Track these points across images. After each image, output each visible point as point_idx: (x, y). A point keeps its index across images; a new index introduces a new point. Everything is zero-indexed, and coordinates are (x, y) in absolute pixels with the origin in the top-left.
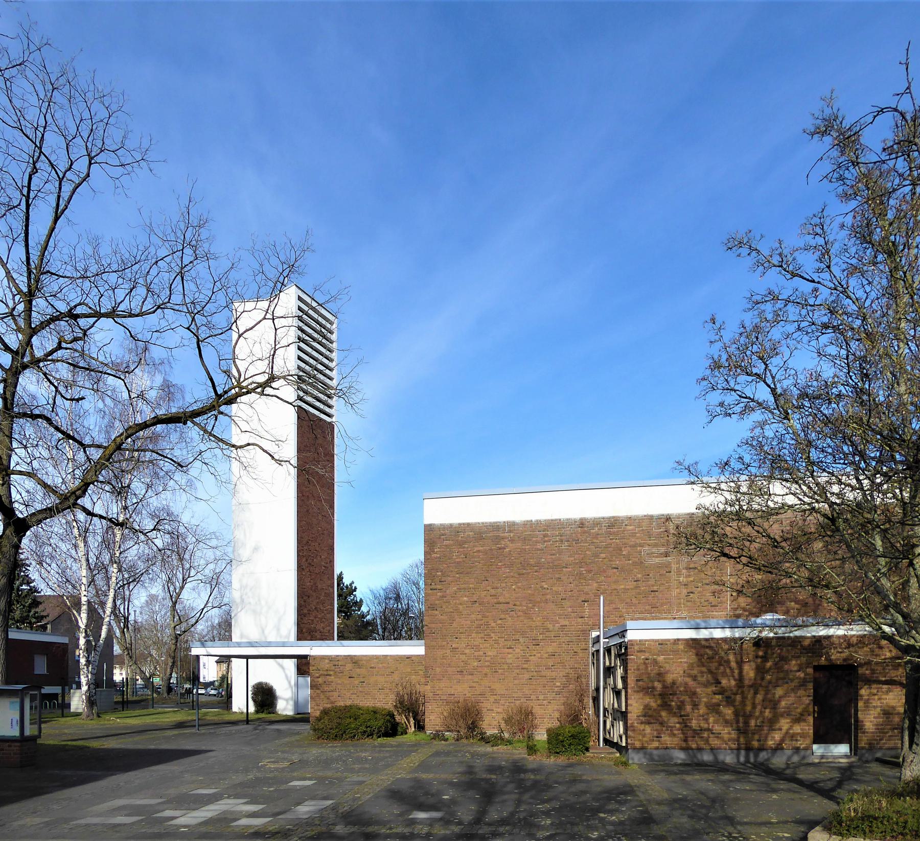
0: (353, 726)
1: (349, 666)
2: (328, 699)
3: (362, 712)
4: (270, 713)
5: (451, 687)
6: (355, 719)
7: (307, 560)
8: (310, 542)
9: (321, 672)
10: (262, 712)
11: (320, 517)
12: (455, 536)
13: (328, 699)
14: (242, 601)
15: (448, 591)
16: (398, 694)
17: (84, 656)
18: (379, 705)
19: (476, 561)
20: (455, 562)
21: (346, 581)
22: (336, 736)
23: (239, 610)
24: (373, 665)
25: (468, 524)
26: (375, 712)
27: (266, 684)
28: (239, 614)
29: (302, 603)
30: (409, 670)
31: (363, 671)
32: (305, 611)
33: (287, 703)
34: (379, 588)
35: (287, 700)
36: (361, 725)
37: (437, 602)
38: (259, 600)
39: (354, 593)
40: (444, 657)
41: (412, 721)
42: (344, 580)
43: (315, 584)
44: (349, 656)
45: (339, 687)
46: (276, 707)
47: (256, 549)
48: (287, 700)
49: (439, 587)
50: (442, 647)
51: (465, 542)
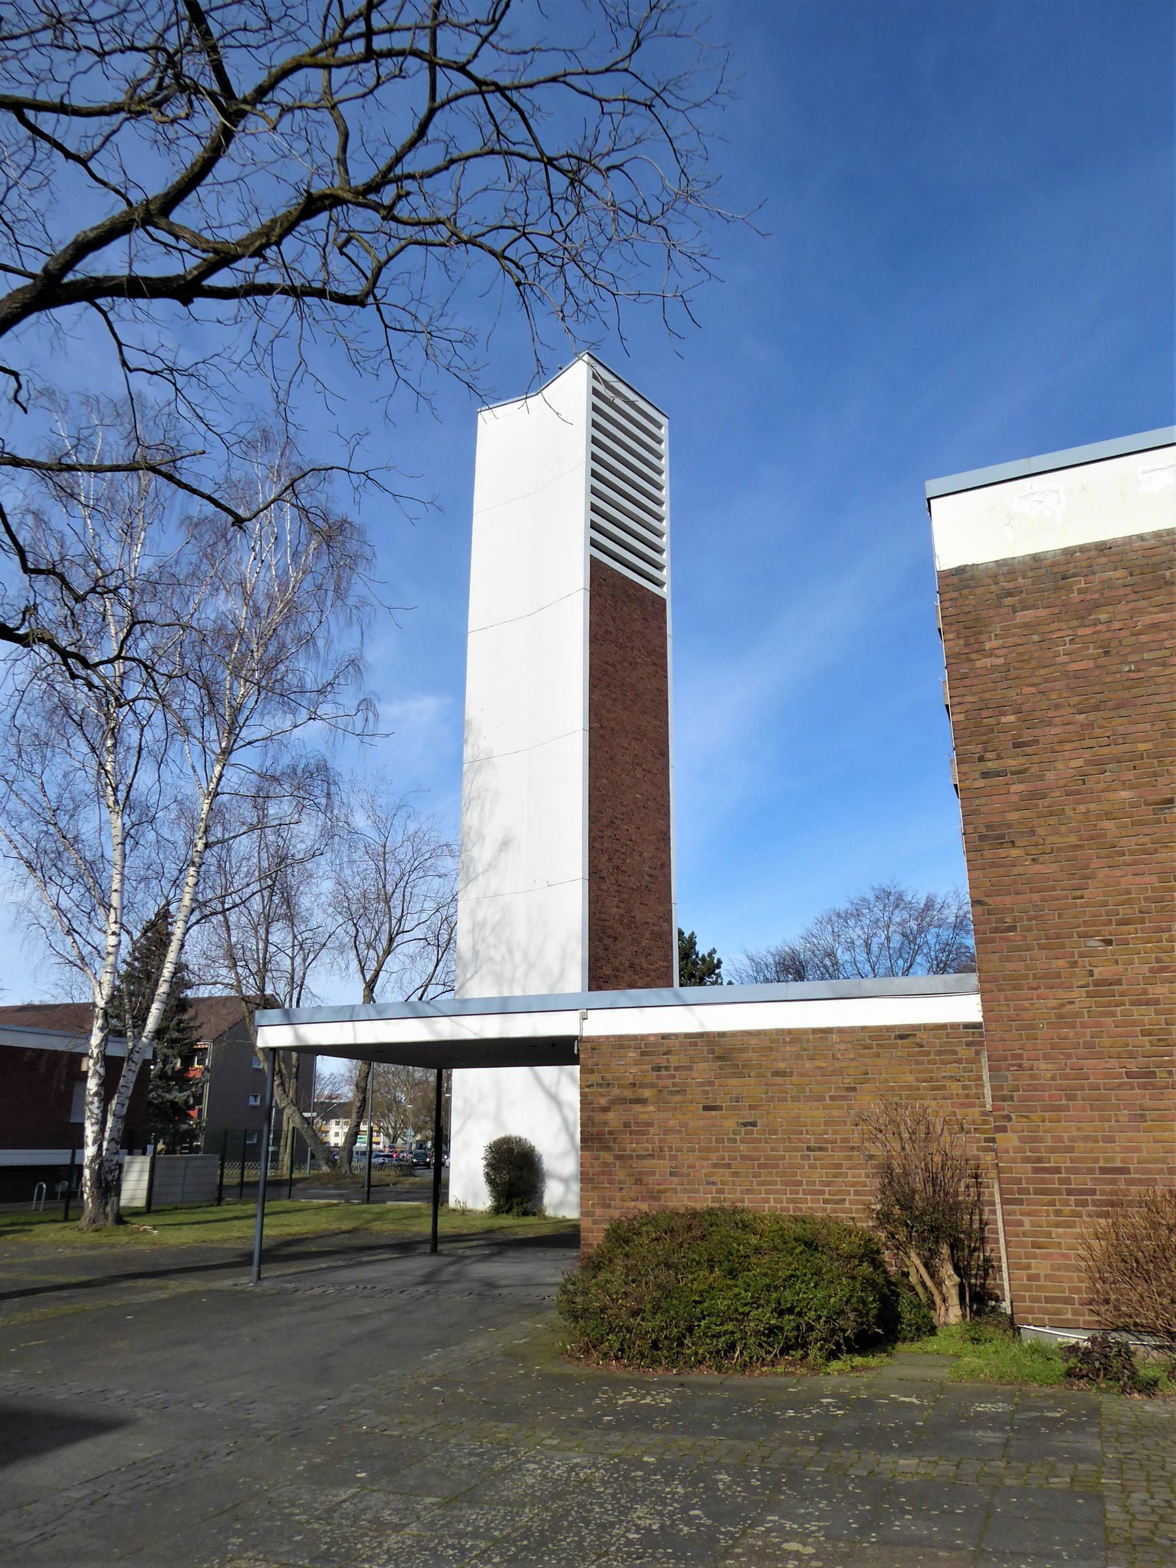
0: (722, 1304)
1: (703, 1070)
2: (638, 1181)
3: (754, 1240)
4: (525, 1213)
5: (1111, 1140)
6: (732, 1273)
7: (610, 859)
8: (618, 822)
9: (616, 1092)
10: (508, 1211)
11: (639, 773)
12: (1057, 589)
13: (638, 1181)
14: (476, 954)
15: (1050, 776)
16: (886, 1170)
17: (96, 1072)
18: (815, 1207)
19: (1152, 662)
20: (1066, 674)
21: (702, 949)
22: (655, 1346)
23: (468, 975)
24: (782, 1065)
25: (1102, 548)
26: (811, 1245)
27: (519, 1142)
28: (468, 985)
29: (602, 953)
30: (910, 1079)
31: (749, 1086)
32: (607, 971)
33: (568, 1189)
34: (764, 952)
35: (565, 1181)
36: (756, 1303)
37: (1013, 816)
38: (510, 951)
39: (717, 971)
40: (1062, 1019)
41: (951, 1280)
42: (697, 948)
43: (629, 911)
44: (701, 1035)
45: (673, 1140)
46: (541, 1198)
47: (505, 845)
48: (565, 1181)
49: (1012, 763)
50: (1052, 979)
51: (1096, 606)
